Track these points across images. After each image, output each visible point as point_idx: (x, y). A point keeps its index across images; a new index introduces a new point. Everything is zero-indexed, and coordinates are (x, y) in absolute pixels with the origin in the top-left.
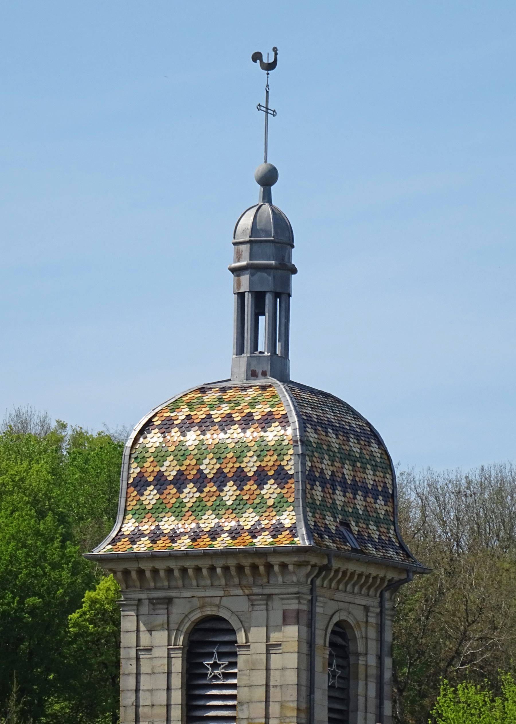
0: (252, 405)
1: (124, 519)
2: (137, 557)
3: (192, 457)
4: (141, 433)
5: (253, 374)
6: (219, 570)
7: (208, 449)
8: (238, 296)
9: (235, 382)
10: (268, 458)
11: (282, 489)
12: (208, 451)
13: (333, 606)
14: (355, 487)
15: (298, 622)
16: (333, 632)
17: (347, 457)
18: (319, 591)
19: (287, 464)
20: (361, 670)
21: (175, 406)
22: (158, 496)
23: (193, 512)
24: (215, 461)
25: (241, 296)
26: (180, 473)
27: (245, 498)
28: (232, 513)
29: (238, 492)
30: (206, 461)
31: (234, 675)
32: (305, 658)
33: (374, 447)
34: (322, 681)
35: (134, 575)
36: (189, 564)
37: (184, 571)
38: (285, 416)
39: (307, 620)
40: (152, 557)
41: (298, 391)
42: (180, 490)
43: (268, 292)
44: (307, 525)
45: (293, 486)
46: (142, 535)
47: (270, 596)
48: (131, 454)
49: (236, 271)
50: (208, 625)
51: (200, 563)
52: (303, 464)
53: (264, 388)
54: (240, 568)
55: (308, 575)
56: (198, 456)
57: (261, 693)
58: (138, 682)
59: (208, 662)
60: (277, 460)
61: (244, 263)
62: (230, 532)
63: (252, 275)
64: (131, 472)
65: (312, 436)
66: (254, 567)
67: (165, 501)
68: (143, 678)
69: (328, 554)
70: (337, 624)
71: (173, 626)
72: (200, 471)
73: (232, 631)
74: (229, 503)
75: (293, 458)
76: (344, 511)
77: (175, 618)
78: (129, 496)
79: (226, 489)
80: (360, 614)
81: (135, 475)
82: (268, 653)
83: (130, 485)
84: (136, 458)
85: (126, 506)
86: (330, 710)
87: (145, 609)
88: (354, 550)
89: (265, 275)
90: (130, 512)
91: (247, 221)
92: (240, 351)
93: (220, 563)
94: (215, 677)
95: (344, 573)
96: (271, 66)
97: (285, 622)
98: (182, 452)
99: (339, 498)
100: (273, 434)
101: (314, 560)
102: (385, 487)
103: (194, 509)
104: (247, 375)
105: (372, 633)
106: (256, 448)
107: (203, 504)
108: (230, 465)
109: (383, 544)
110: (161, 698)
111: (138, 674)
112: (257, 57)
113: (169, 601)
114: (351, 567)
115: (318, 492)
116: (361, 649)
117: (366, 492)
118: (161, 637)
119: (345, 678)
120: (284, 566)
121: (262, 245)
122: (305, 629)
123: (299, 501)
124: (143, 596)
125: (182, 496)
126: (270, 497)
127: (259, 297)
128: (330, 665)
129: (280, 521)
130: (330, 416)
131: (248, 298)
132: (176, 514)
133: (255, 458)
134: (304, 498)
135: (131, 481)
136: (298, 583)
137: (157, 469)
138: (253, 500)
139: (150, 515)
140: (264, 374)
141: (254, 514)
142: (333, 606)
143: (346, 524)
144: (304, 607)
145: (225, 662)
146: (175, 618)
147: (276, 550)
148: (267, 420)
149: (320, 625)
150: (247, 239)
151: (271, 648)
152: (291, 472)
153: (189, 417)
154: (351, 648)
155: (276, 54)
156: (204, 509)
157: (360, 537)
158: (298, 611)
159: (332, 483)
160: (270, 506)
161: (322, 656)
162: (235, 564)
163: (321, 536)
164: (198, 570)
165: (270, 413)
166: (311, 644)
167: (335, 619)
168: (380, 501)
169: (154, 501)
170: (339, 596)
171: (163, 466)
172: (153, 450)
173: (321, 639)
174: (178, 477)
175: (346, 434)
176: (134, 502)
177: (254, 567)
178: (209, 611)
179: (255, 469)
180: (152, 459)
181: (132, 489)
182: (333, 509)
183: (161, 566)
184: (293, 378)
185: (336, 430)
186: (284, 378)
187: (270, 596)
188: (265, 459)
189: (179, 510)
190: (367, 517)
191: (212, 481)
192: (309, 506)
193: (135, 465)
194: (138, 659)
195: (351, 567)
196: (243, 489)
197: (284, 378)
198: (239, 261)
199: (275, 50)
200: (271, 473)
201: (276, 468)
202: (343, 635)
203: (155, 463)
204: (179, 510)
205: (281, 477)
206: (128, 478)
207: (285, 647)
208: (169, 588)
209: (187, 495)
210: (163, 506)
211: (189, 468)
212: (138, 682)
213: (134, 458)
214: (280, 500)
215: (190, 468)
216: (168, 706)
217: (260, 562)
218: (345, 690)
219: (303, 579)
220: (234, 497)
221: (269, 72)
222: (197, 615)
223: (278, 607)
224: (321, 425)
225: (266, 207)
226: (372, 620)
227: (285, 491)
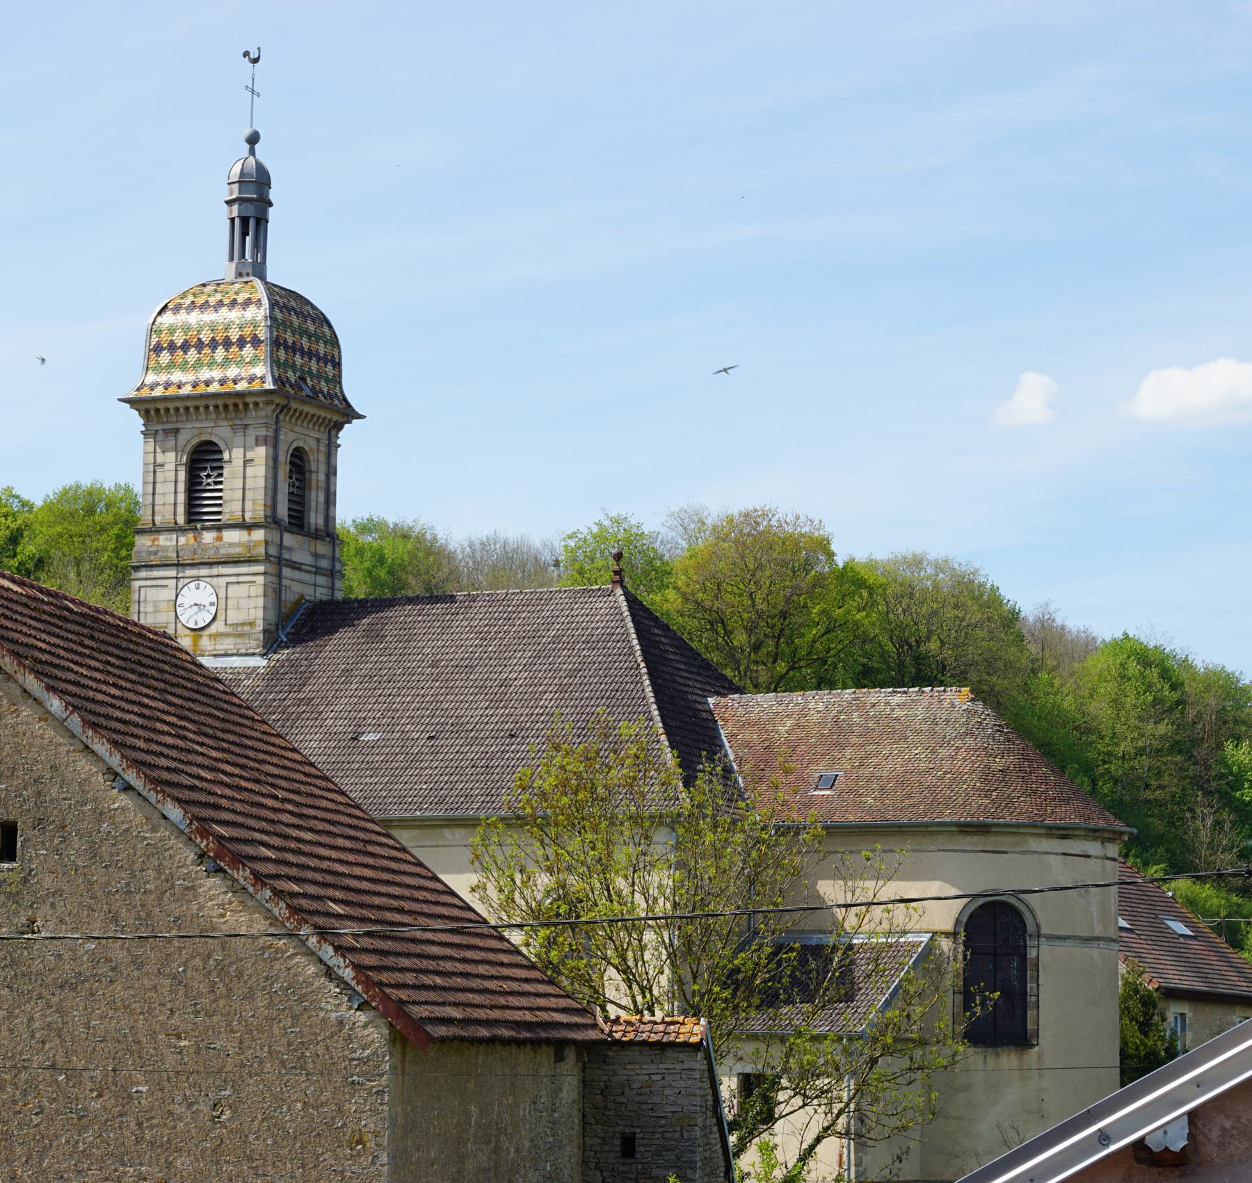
0: (237, 293)
2: (154, 400)
4: (160, 313)
5: (240, 275)
9: (228, 280)
13: (291, 436)
14: (310, 354)
15: (266, 444)
16: (292, 455)
17: (304, 332)
18: (282, 424)
20: (314, 483)
21: (183, 296)
25: (232, 220)
26: (186, 341)
31: (221, 483)
32: (271, 470)
33: (326, 329)
34: (284, 488)
35: (152, 412)
36: (190, 404)
37: (187, 409)
38: (259, 300)
39: (273, 443)
40: (165, 399)
41: (271, 288)
42: (185, 353)
44: (273, 376)
46: (159, 384)
47: (246, 426)
49: (229, 203)
50: (204, 448)
51: (198, 403)
52: (271, 333)
53: (246, 283)
54: (226, 407)
55: (274, 411)
58: (154, 488)
59: (203, 474)
61: (234, 197)
62: (220, 381)
65: (279, 315)
66: (236, 406)
68: (158, 486)
69: (288, 397)
70: (296, 449)
71: (179, 448)
73: (220, 452)
76: (301, 370)
77: (181, 442)
80: (313, 444)
82: (245, 466)
86: (290, 509)
87: (160, 437)
88: (308, 396)
91: (237, 169)
92: (231, 259)
93: (211, 403)
94: (208, 484)
95: (301, 413)
96: (256, 61)
97: (257, 444)
99: (298, 360)
100: (251, 313)
101: (278, 400)
102: (333, 356)
105: (322, 458)
109: (329, 396)
110: (171, 499)
111: (154, 483)
112: (246, 54)
113: (177, 431)
114: (306, 409)
115: (282, 354)
116: (313, 468)
117: (319, 359)
118: (171, 456)
119: (302, 488)
120: (256, 404)
122: (271, 450)
124: (159, 427)
127: (245, 221)
128: (290, 478)
129: (253, 372)
130: (294, 304)
131: (237, 221)
134: (271, 357)
136: (266, 416)
140: (248, 275)
142: (291, 436)
143: (304, 380)
144: (271, 434)
145: (215, 473)
146: (181, 442)
148: (247, 303)
149: (283, 448)
151: (247, 462)
153: (193, 302)
154: (307, 468)
156: (202, 365)
157: (313, 389)
158: (266, 436)
159: (293, 349)
161: (284, 471)
163: (283, 383)
164: (197, 408)
165: (249, 299)
166: (275, 460)
167: (295, 445)
168: (329, 366)
170: (297, 429)
173: (284, 458)
175: (305, 317)
177: (236, 406)
178: (205, 438)
182: (293, 367)
183: (171, 405)
184: (270, 278)
185: (297, 314)
186: (262, 277)
187: (246, 426)
190: (319, 376)
192: (275, 362)
194: (155, 472)
195: (306, 409)
197: (262, 277)
202: (301, 458)
204: (184, 367)
205: (256, 342)
207: (256, 462)
208: (177, 421)
212: (154, 488)
216: (175, 504)
217: (240, 402)
218: (302, 496)
219: (270, 414)
222: (196, 441)
223: (252, 434)
224: (285, 308)
225: (252, 160)
226: (323, 448)
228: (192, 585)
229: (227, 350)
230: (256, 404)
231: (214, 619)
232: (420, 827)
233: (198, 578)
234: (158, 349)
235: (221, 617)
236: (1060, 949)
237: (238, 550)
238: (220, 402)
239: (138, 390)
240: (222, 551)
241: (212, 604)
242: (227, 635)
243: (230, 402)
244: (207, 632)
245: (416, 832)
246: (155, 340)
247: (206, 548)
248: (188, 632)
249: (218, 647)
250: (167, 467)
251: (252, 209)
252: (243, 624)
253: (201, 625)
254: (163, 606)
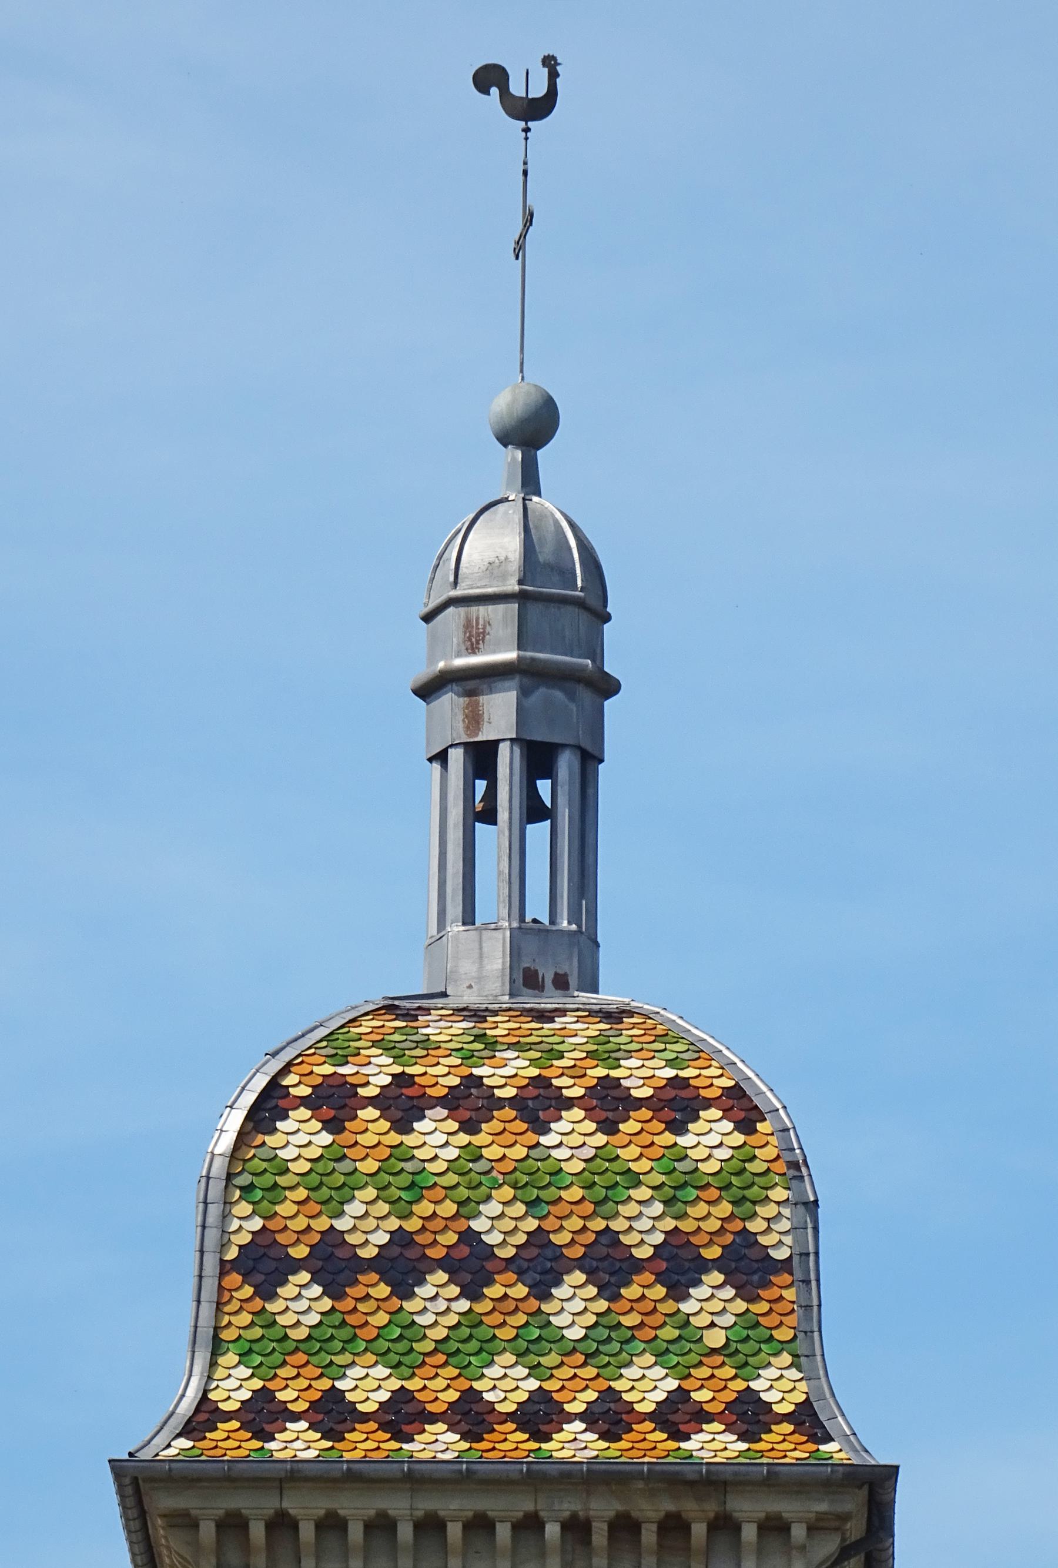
1: (213, 1364)
3: (440, 1193)
5: (531, 981)
6: (552, 1530)
7: (494, 1173)
8: (465, 752)
10: (702, 1209)
11: (749, 1301)
12: (495, 1180)
19: (768, 1230)
22: (327, 1303)
23: (449, 1355)
24: (519, 1209)
27: (629, 1321)
28: (584, 1364)
29: (602, 1305)
30: (493, 1208)
42: (403, 1290)
43: (564, 746)
45: (790, 1294)
48: (230, 1177)
56: (463, 1193)
60: (732, 1216)
63: (524, 693)
64: (235, 1225)
67: (351, 1319)
72: (469, 1237)
74: (575, 1333)
75: (786, 1212)
78: (226, 1296)
79: (561, 1292)
81: (245, 1238)
83: (228, 1266)
84: (247, 1189)
85: (217, 1329)
89: (558, 695)
90: (231, 1346)
98: (405, 1180)
103: (453, 1346)
104: (512, 981)
106: (658, 1179)
107: (484, 1332)
108: (575, 1223)
112: (489, 78)
121: (553, 609)
123: (812, 1337)
125: (409, 1306)
126: (713, 1325)
132: (394, 1358)
133: (658, 1208)
135: (232, 1253)
137: (322, 1224)
138: (656, 1328)
139: (301, 1358)
141: (659, 1372)
147: (776, 1474)
150: (512, 586)
152: (781, 1254)
155: (553, 75)
156: (488, 1349)
160: (714, 1351)
162: (612, 1514)
169: (314, 1319)
171: (341, 1214)
172: (303, 1166)
174: (396, 1251)
176: (245, 1318)
177: (674, 1527)
179: (658, 1238)
180: (301, 1194)
181: (235, 1278)
188: (693, 1211)
189: (402, 1347)
191: (513, 1267)
193: (244, 1208)
196: (620, 1296)
198: (473, 650)
199: (550, 63)
200: (713, 1253)
201: (729, 1238)
203: (313, 1208)
206: (224, 1246)
209: (428, 1305)
210: (345, 1333)
211: (431, 1226)
213: (241, 1188)
214: (745, 1333)
215: (437, 1224)
220: (590, 1319)
221: (530, 124)
227: (763, 1307)
229: (609, 1291)
230: (774, 1528)
234: (262, 1265)
238: (602, 1508)
239: (189, 1430)
243: (650, 1510)
246: (246, 1223)
251: (539, 704)
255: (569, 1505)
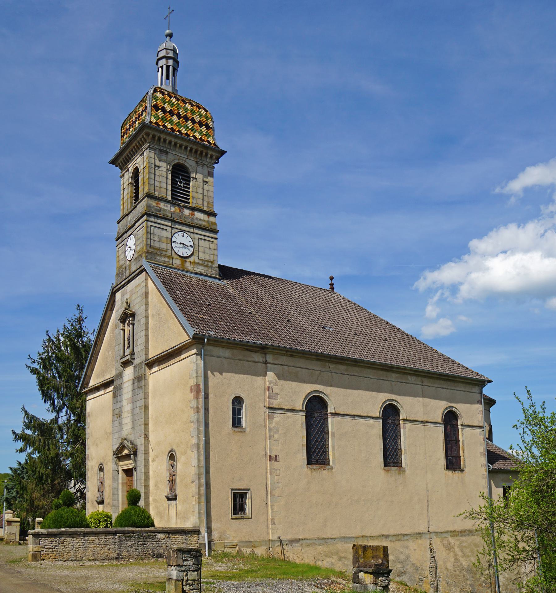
57: (201, 196)
72: (178, 113)
113: (167, 153)
131: (171, 68)
177: (201, 153)
178: (181, 162)
217: (205, 151)
222: (176, 162)
228: (180, 233)
231: (192, 255)
232: (401, 373)
233: (183, 231)
235: (196, 254)
236: (108, 378)
237: (204, 223)
240: (196, 221)
241: (191, 246)
242: (200, 264)
244: (188, 260)
245: (398, 375)
247: (186, 217)
248: (178, 257)
249: (195, 269)
250: (162, 169)
252: (208, 261)
253: (185, 255)
254: (164, 240)
255: (191, 146)
